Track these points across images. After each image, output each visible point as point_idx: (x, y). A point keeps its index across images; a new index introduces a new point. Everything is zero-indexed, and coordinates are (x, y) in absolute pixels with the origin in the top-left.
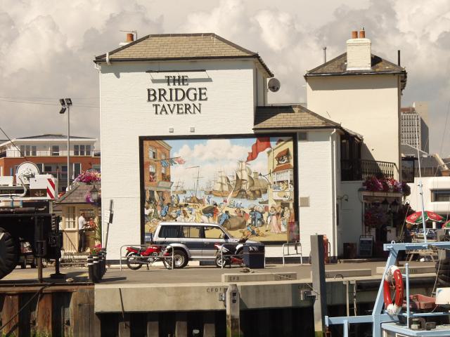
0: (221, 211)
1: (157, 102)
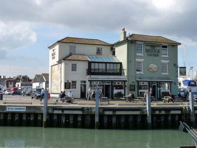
1: (148, 53)
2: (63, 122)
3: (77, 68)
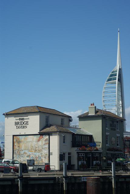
1: (17, 126)
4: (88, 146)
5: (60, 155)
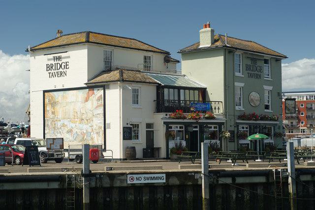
0: (75, 131)
1: (50, 71)
2: (232, 197)
3: (139, 97)
4: (192, 109)
5: (124, 128)
